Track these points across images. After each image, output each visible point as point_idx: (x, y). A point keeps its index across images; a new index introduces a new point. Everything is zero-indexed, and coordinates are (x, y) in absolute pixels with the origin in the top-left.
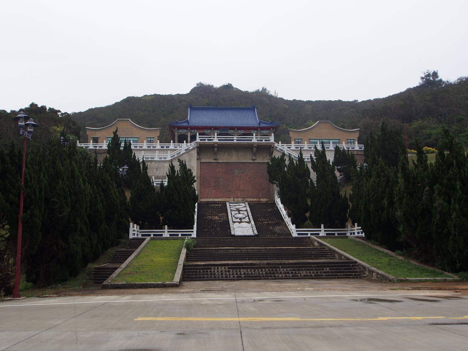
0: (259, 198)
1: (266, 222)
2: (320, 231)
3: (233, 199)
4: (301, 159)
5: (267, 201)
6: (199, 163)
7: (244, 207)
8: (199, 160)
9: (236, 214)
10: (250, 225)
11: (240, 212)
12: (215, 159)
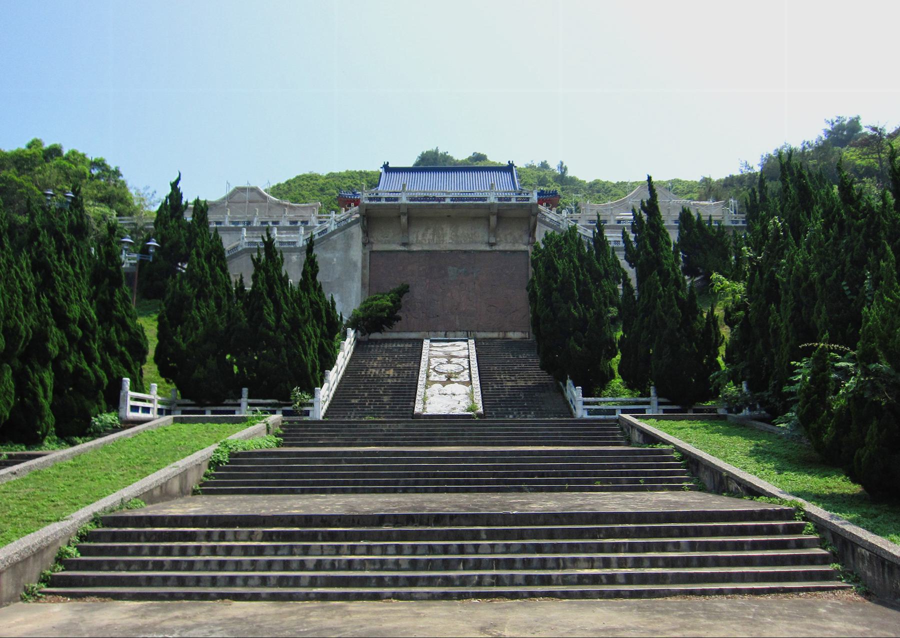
0: (506, 332)
1: (510, 384)
2: (648, 403)
3: (443, 333)
4: (600, 241)
5: (523, 339)
6: (368, 252)
7: (464, 349)
8: (367, 246)
9: (441, 364)
10: (468, 389)
11: (453, 360)
12: (404, 244)
